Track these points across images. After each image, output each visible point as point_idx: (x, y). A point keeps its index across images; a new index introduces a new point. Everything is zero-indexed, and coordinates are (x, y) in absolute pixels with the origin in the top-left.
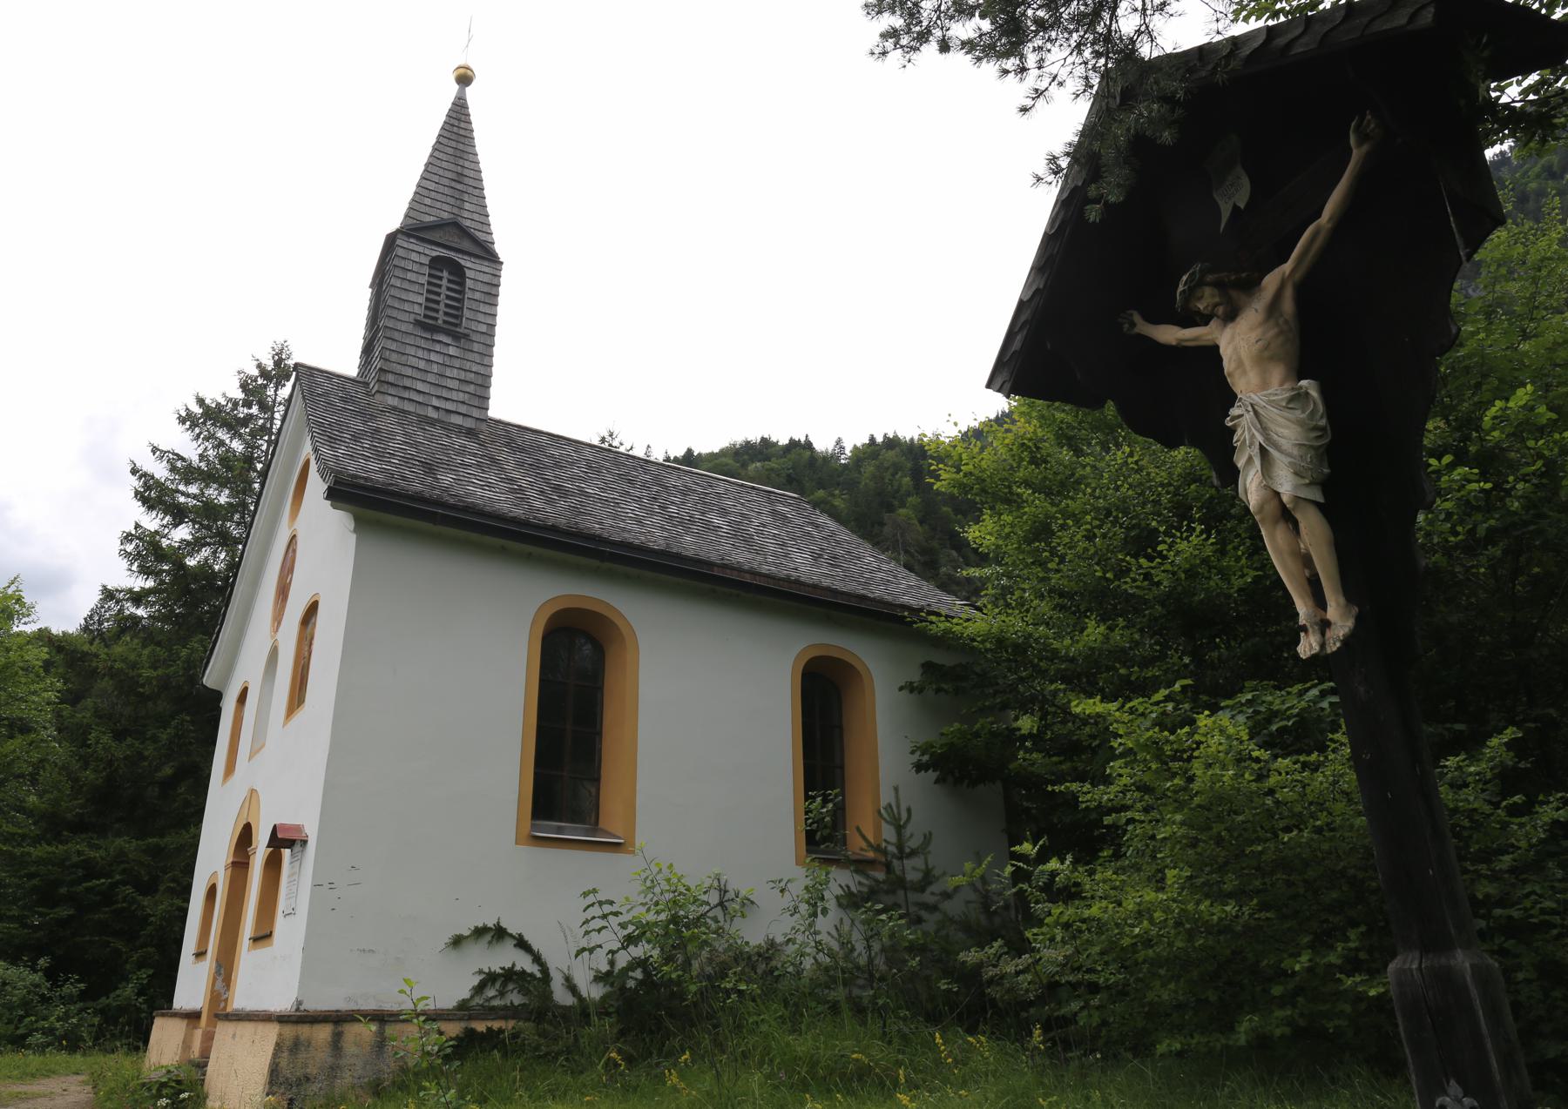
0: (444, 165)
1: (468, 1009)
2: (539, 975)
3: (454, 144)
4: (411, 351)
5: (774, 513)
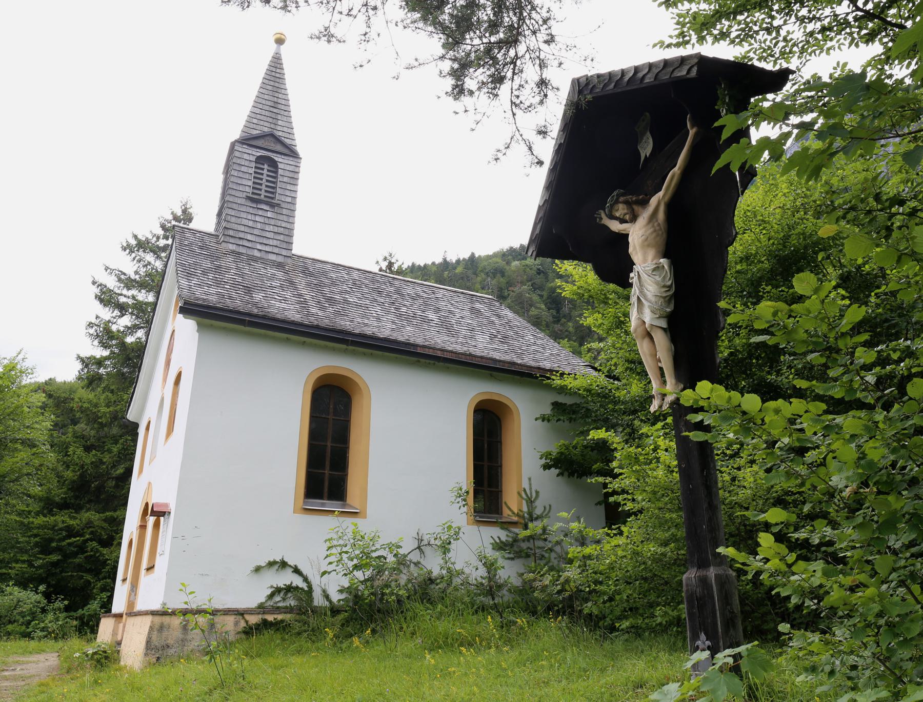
1: (264, 608)
2: (306, 589)
3: (272, 83)
4: (244, 215)
5: (473, 310)
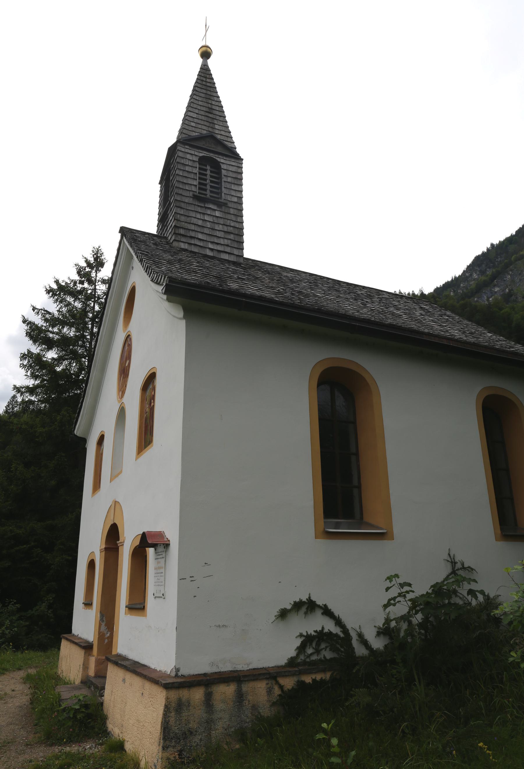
0: (200, 103)
2: (342, 635)
3: (204, 91)
4: (193, 214)
